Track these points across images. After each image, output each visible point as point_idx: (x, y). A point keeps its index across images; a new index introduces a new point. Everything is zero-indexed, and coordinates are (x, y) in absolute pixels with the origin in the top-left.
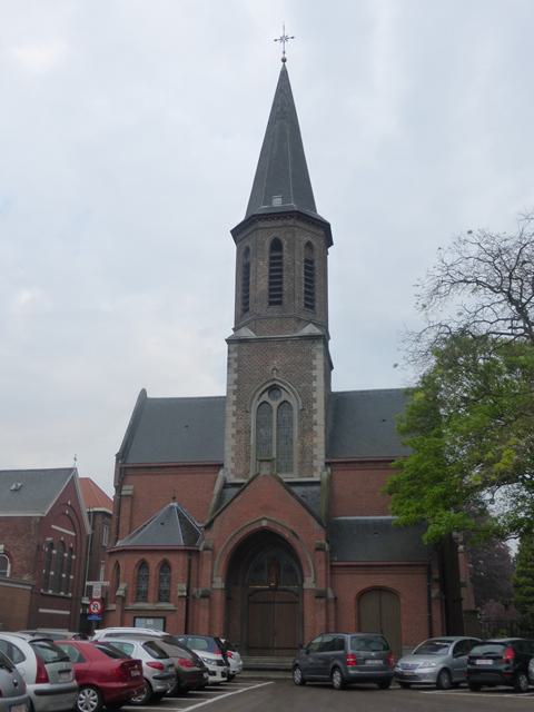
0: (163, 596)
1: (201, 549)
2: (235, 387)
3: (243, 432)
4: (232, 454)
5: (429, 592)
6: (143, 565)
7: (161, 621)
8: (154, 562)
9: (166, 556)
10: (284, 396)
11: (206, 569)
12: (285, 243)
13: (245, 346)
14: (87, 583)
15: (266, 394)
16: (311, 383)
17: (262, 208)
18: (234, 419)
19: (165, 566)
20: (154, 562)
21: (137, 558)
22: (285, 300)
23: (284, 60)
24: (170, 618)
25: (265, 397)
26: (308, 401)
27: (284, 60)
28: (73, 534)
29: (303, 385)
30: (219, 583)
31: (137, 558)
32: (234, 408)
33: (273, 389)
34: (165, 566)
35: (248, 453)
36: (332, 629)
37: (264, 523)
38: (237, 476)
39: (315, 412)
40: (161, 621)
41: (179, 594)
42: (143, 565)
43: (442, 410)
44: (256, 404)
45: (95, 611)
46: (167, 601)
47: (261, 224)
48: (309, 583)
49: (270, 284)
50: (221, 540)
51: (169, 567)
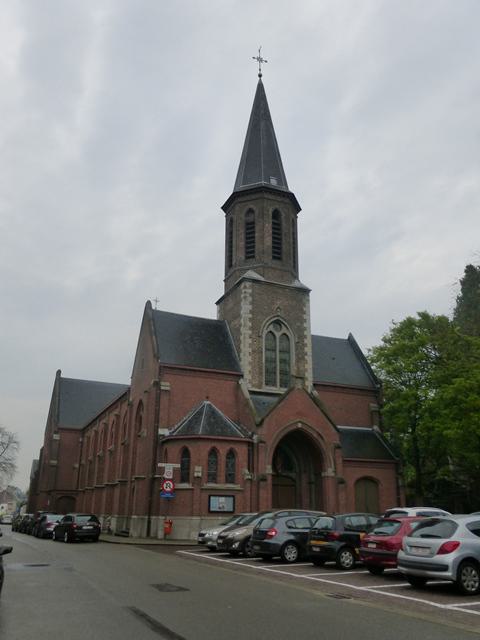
0: (230, 478)
1: (255, 442)
2: (250, 316)
3: (256, 352)
4: (249, 368)
5: (397, 482)
6: (213, 452)
7: (231, 499)
8: (223, 450)
9: (232, 446)
10: (284, 330)
11: (262, 456)
12: (283, 215)
13: (257, 286)
14: (159, 465)
15: (271, 326)
16: (302, 323)
17: (242, 187)
18: (250, 341)
19: (231, 454)
20: (223, 450)
21: (209, 446)
22: (284, 258)
23: (260, 76)
24: (238, 497)
25: (271, 328)
26: (300, 345)
27: (260, 76)
28: (339, 427)
29: (298, 324)
30: (269, 470)
31: (209, 446)
32: (250, 332)
33: (278, 323)
34: (231, 454)
35: (261, 369)
36: (248, 509)
37: (300, 425)
38: (253, 386)
39: (306, 345)
40: (231, 499)
41: (196, 475)
42: (213, 452)
43: (433, 353)
44: (265, 332)
45: (168, 489)
46: (232, 482)
47: (240, 200)
48: (330, 472)
49: (274, 243)
50: (269, 436)
51: (234, 456)
